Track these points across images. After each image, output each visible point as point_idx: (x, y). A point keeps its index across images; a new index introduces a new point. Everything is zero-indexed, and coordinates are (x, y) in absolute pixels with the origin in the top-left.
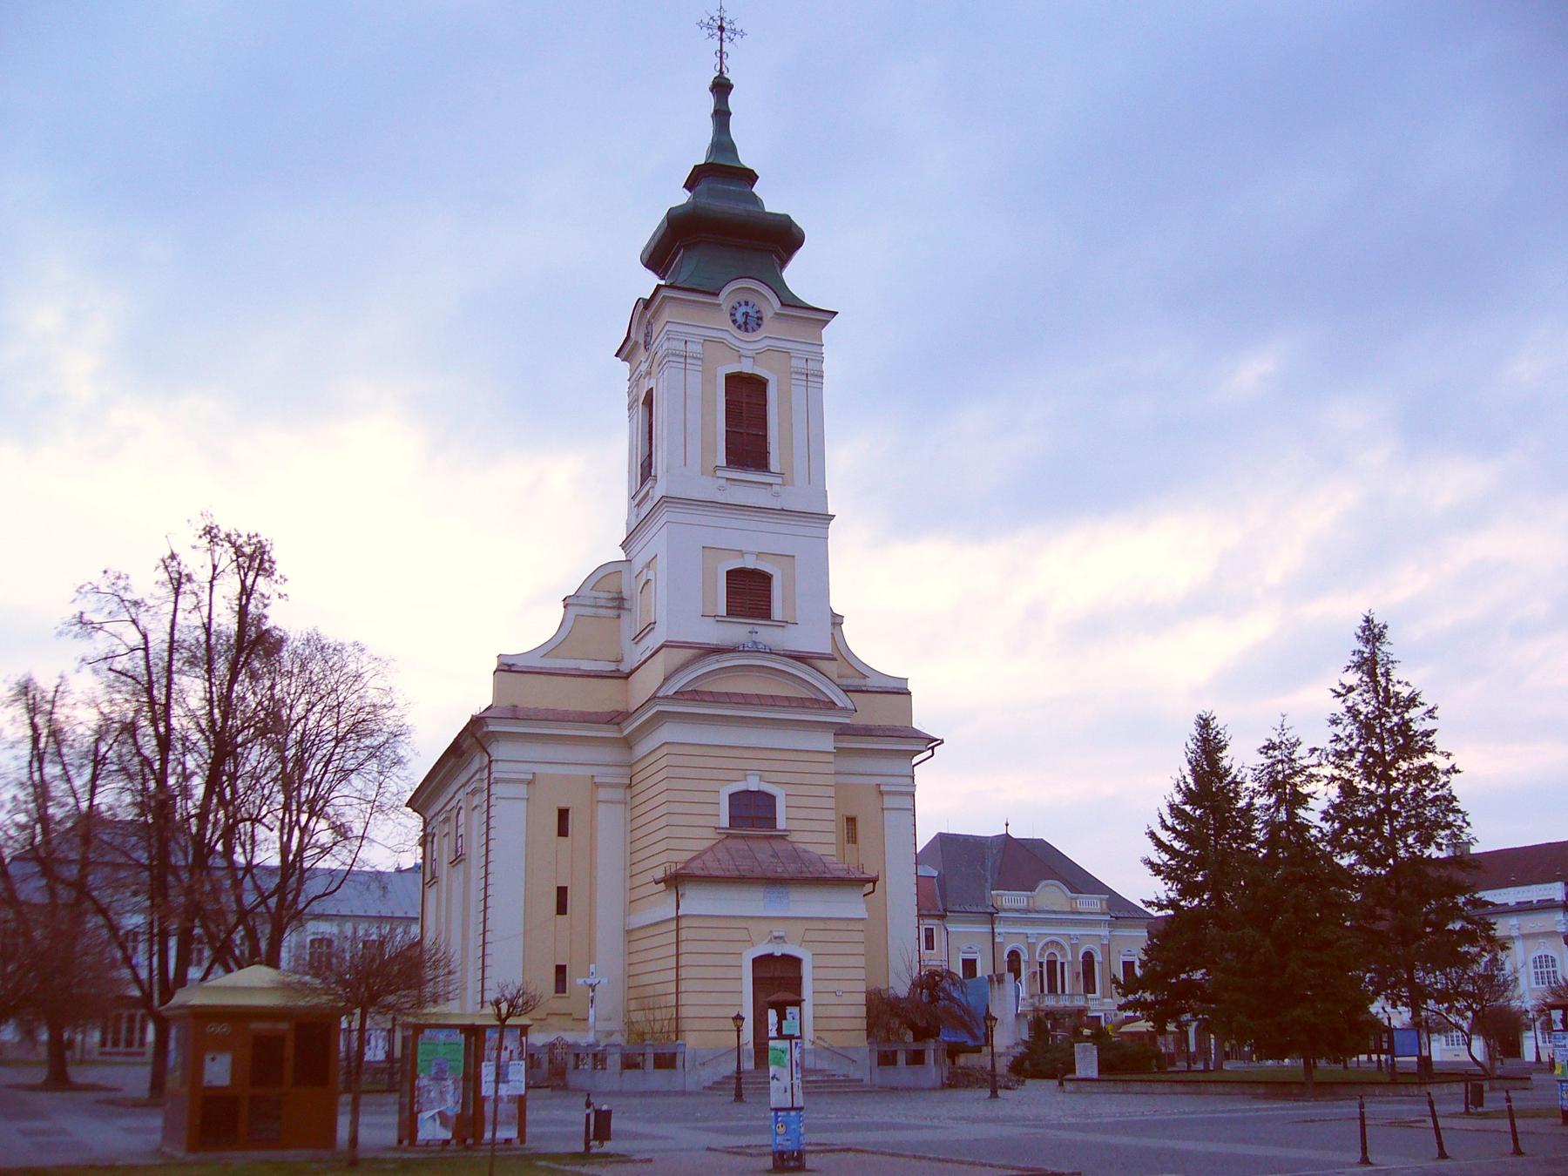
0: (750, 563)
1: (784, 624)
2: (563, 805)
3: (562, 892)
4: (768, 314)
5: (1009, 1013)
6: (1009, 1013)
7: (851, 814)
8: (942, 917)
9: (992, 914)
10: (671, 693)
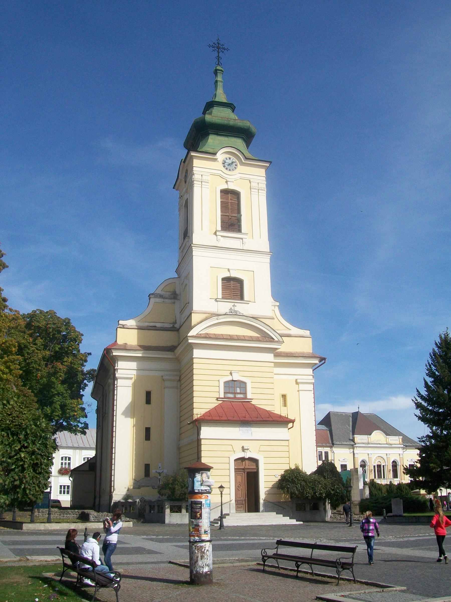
0: (234, 274)
1: (248, 302)
5: (360, 490)
6: (360, 490)
7: (284, 393)
8: (331, 447)
9: (353, 445)
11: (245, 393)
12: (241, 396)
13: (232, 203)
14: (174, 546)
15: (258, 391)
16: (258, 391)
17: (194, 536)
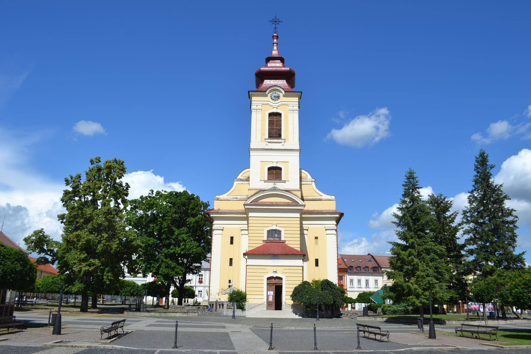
0: (274, 165)
1: (285, 182)
2: (232, 236)
3: (231, 260)
4: (281, 95)
7: (316, 236)
10: (249, 202)
15: (289, 236)
16: (289, 236)
17: (502, 269)
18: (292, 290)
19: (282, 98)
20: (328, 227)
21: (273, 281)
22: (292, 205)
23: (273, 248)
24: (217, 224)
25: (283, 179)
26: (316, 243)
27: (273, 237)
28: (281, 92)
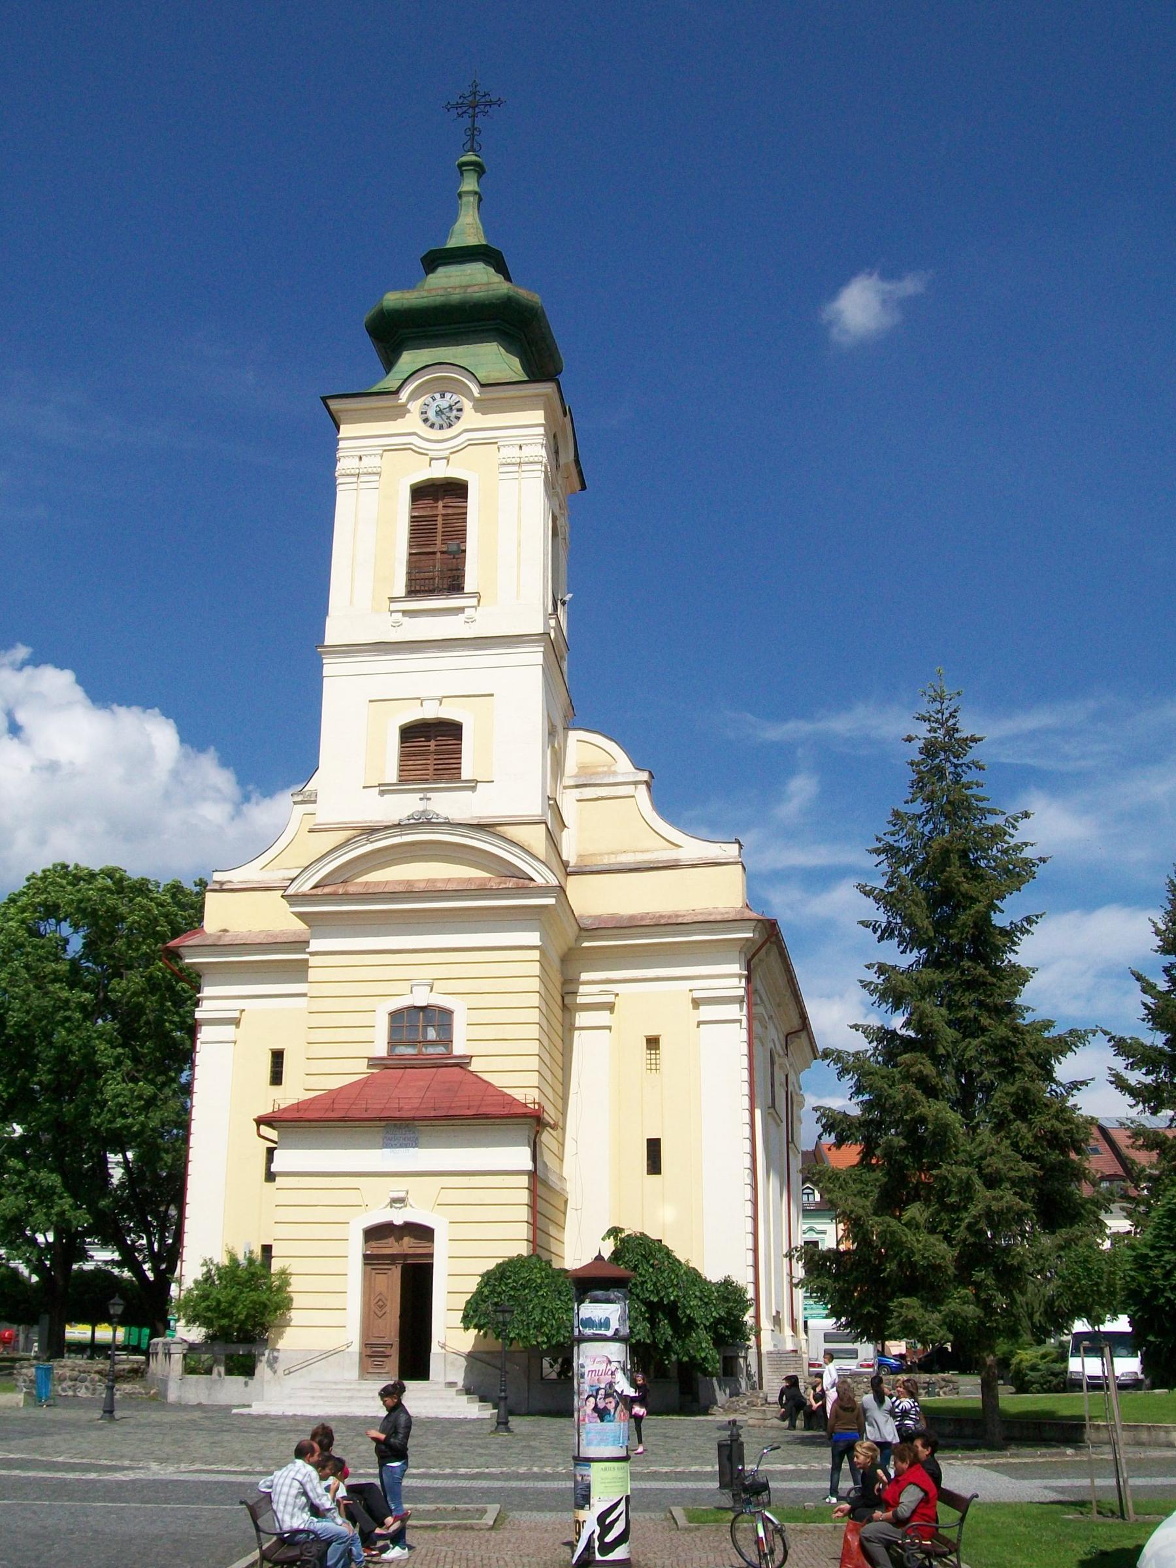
0: (430, 712)
1: (472, 785)
2: (277, 1046)
7: (653, 1033)
11: (448, 1042)
12: (441, 1050)
13: (448, 515)
14: (1046, 1488)
18: (473, 1284)
19: (470, 417)
20: (705, 989)
21: (391, 1247)
22: (505, 890)
23: (420, 1091)
24: (214, 1001)
25: (466, 774)
26: (653, 1067)
27: (413, 1043)
28: (468, 393)
